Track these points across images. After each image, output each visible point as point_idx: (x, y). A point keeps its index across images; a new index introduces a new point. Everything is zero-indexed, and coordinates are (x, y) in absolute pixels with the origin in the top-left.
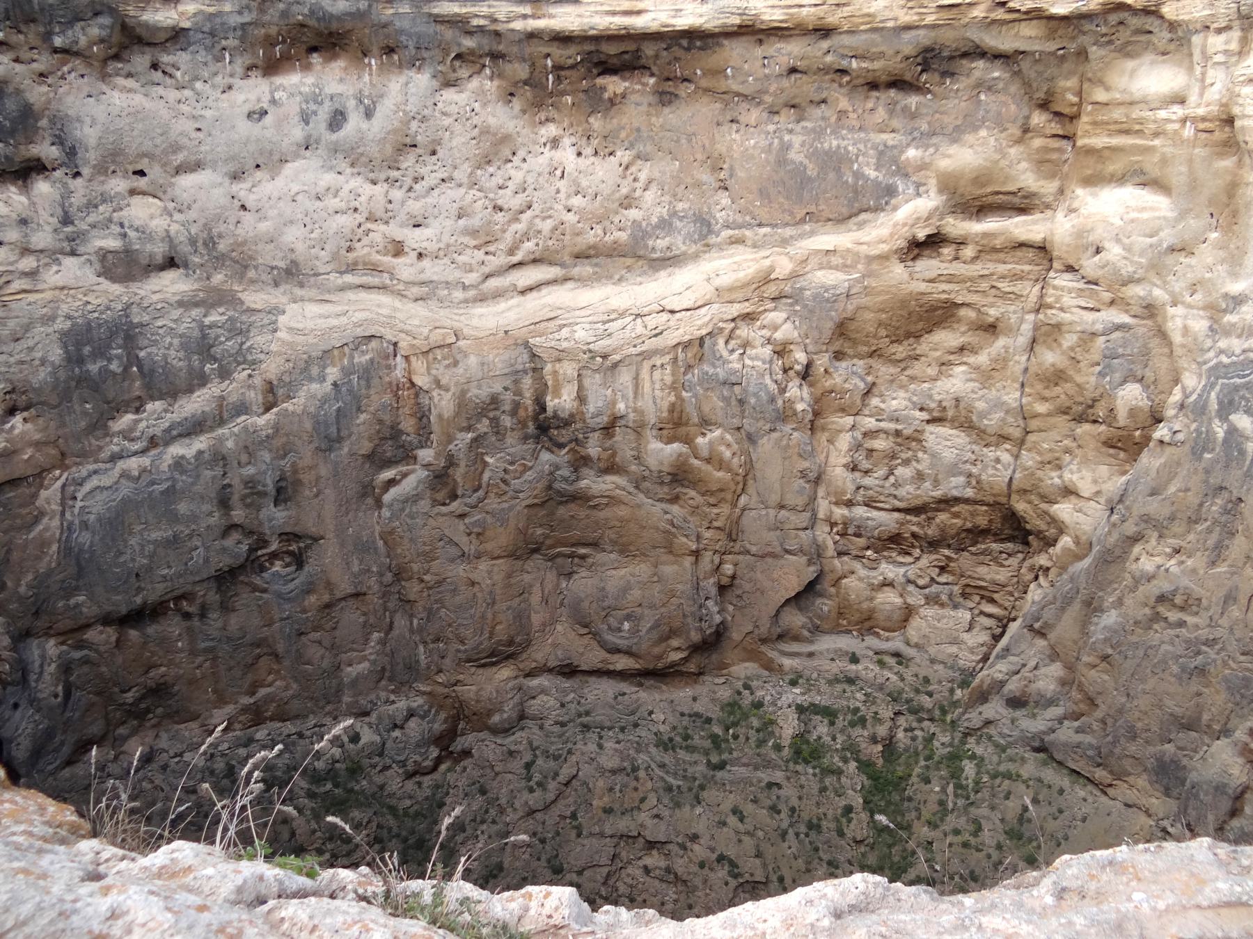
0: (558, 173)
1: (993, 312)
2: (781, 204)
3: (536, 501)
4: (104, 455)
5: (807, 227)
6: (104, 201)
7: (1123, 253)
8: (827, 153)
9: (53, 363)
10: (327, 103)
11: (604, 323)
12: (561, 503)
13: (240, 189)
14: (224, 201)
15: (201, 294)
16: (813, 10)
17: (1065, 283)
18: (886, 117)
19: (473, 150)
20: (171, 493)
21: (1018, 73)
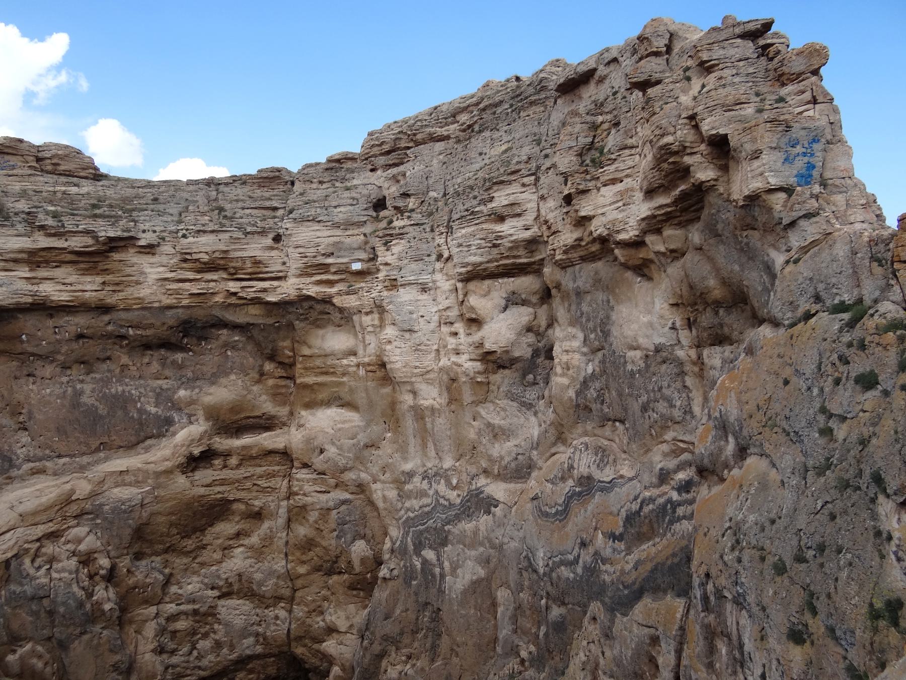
5: (102, 455)
8: (114, 396)
16: (94, 294)
17: (304, 476)
18: (160, 368)
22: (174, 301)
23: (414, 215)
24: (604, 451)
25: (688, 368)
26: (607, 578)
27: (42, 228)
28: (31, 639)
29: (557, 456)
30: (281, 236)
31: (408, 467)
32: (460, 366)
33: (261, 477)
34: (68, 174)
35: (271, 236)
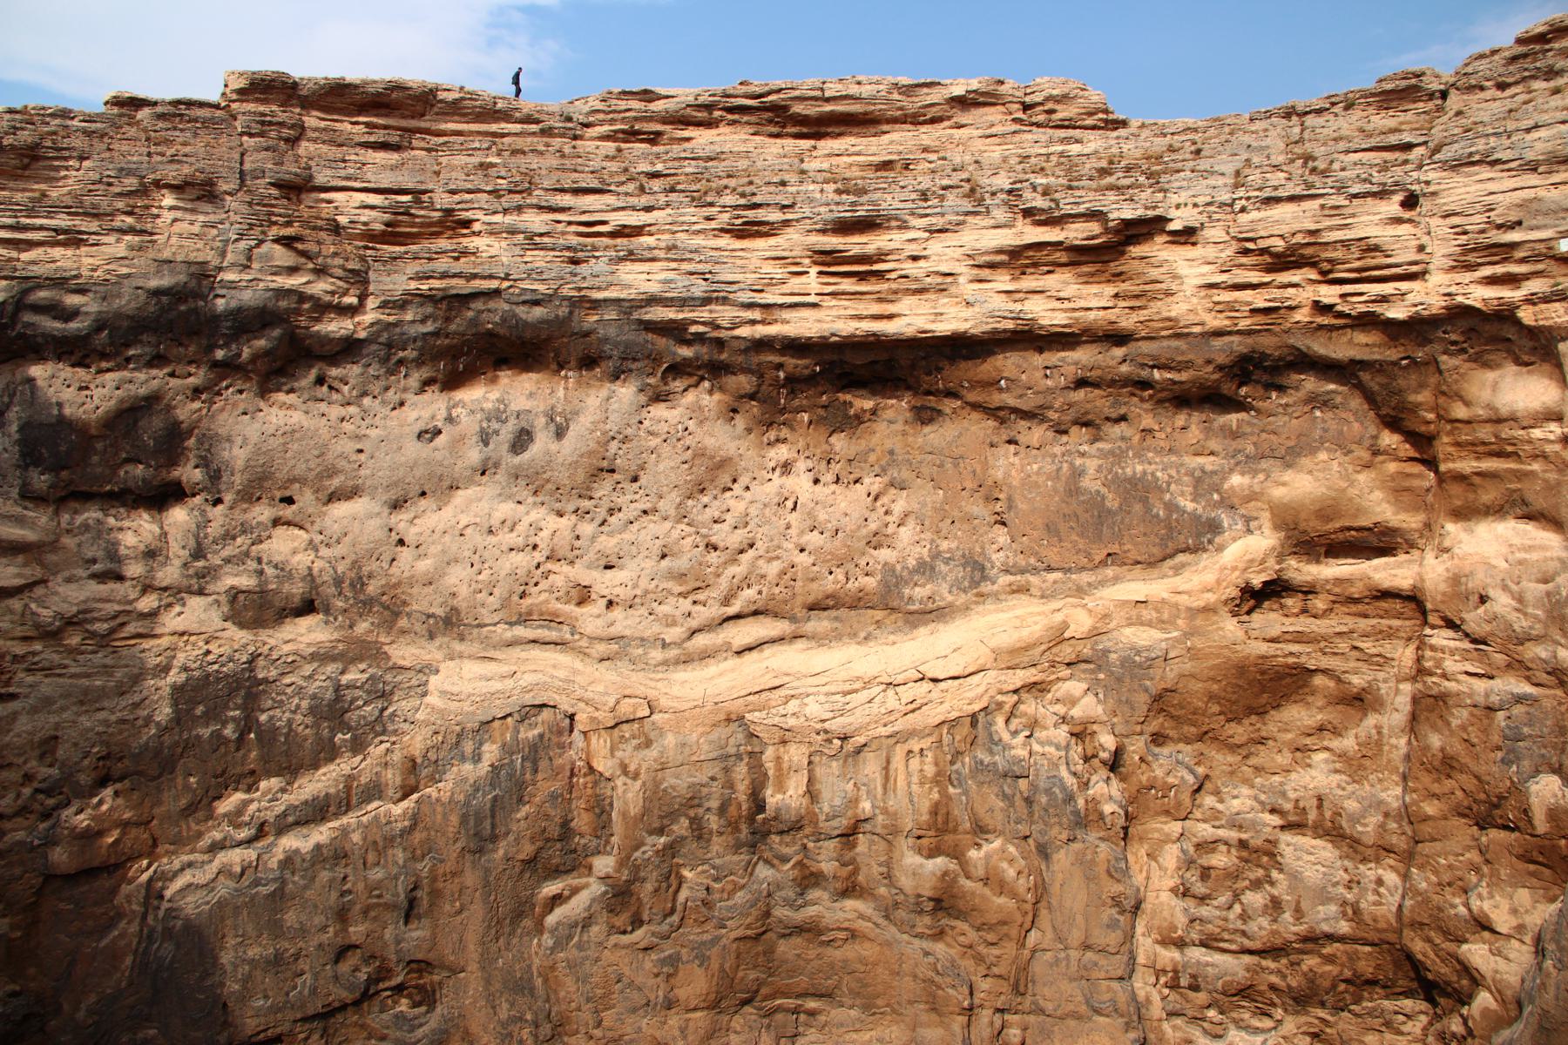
0: (789, 504)
2: (1075, 543)
3: (749, 932)
4: (205, 842)
5: (1110, 572)
6: (244, 532)
7: (1514, 603)
9: (158, 724)
10: (512, 421)
11: (845, 694)
12: (784, 936)
13: (401, 519)
14: (381, 534)
15: (341, 646)
16: (1102, 313)
17: (1445, 642)
18: (1202, 436)
19: (683, 476)
20: (279, 897)
22: (1227, 322)
28: (1002, 833)
30: (1417, 197)
35: (1398, 198)
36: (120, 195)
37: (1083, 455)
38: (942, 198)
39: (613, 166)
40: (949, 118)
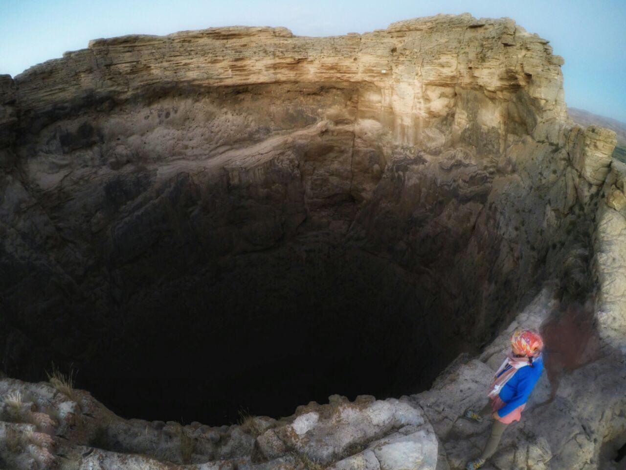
1: (343, 148)
5: (295, 129)
8: (299, 111)
11: (244, 159)
13: (144, 138)
21: (343, 93)
23: (407, 57)
24: (467, 154)
25: (501, 136)
26: (460, 193)
27: (278, 56)
29: (450, 151)
31: (397, 144)
32: (420, 114)
33: (344, 139)
34: (283, 36)
35: (353, 58)
36: (72, 77)
37: (289, 106)
38: (259, 53)
39: (182, 49)
40: (257, 34)
